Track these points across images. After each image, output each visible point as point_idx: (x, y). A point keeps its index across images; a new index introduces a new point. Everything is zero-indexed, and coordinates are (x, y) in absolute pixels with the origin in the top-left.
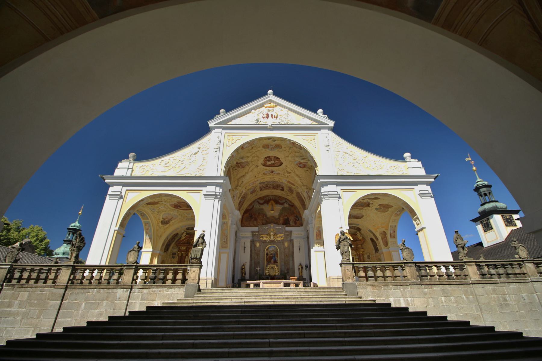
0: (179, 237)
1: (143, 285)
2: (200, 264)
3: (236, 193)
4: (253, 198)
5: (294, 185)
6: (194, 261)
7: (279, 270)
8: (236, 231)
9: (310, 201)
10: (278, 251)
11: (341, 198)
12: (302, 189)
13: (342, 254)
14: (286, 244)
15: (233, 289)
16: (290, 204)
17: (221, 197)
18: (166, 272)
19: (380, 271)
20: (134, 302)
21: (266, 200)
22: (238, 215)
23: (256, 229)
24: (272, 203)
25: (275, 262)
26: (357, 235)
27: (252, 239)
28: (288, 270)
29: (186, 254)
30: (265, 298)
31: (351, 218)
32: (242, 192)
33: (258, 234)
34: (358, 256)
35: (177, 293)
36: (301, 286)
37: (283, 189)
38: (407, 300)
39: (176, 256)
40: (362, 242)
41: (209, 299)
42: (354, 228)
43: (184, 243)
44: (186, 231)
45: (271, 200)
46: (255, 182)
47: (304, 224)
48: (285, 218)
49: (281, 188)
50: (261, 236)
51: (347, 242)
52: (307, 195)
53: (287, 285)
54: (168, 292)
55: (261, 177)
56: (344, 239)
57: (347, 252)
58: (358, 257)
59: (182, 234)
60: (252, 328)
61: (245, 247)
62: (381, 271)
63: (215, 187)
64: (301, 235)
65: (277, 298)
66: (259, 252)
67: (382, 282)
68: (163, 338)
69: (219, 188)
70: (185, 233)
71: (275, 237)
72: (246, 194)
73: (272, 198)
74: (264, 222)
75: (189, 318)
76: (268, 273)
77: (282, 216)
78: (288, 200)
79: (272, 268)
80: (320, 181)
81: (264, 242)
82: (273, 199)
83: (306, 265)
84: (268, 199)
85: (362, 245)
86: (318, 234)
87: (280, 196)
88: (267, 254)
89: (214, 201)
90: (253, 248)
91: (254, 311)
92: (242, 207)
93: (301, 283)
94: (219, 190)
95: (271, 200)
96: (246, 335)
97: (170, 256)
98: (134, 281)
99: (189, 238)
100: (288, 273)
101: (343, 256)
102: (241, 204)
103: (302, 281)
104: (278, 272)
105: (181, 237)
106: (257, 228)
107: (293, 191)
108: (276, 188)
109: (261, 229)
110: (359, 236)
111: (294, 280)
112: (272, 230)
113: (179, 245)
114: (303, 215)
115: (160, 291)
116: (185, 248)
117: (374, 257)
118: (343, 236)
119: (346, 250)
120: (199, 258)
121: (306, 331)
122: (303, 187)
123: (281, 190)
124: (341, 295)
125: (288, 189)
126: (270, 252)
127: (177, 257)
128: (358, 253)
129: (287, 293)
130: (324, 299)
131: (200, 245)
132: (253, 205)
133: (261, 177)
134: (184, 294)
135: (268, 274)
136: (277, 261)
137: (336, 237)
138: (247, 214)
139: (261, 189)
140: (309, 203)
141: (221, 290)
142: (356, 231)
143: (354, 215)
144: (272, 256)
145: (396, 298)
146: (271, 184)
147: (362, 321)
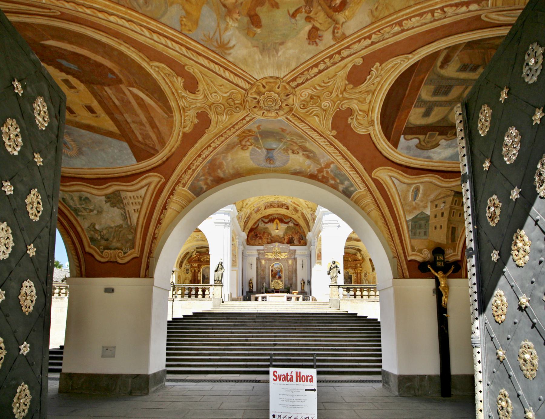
4: (259, 216)
10: (282, 268)
14: (290, 262)
21: (271, 219)
22: (244, 235)
23: (261, 247)
25: (280, 277)
28: (291, 284)
33: (263, 252)
43: (195, 261)
45: (275, 218)
47: (308, 244)
53: (289, 299)
59: (193, 252)
60: (264, 325)
70: (195, 251)
72: (251, 214)
73: (276, 217)
74: (269, 241)
75: (224, 319)
81: (269, 260)
85: (361, 264)
88: (272, 271)
92: (247, 226)
93: (301, 297)
95: (275, 218)
98: (174, 296)
100: (291, 287)
102: (246, 223)
106: (263, 247)
110: (359, 256)
112: (277, 249)
116: (197, 265)
123: (286, 209)
135: (273, 288)
138: (252, 233)
140: (313, 226)
142: (356, 251)
147: (333, 323)
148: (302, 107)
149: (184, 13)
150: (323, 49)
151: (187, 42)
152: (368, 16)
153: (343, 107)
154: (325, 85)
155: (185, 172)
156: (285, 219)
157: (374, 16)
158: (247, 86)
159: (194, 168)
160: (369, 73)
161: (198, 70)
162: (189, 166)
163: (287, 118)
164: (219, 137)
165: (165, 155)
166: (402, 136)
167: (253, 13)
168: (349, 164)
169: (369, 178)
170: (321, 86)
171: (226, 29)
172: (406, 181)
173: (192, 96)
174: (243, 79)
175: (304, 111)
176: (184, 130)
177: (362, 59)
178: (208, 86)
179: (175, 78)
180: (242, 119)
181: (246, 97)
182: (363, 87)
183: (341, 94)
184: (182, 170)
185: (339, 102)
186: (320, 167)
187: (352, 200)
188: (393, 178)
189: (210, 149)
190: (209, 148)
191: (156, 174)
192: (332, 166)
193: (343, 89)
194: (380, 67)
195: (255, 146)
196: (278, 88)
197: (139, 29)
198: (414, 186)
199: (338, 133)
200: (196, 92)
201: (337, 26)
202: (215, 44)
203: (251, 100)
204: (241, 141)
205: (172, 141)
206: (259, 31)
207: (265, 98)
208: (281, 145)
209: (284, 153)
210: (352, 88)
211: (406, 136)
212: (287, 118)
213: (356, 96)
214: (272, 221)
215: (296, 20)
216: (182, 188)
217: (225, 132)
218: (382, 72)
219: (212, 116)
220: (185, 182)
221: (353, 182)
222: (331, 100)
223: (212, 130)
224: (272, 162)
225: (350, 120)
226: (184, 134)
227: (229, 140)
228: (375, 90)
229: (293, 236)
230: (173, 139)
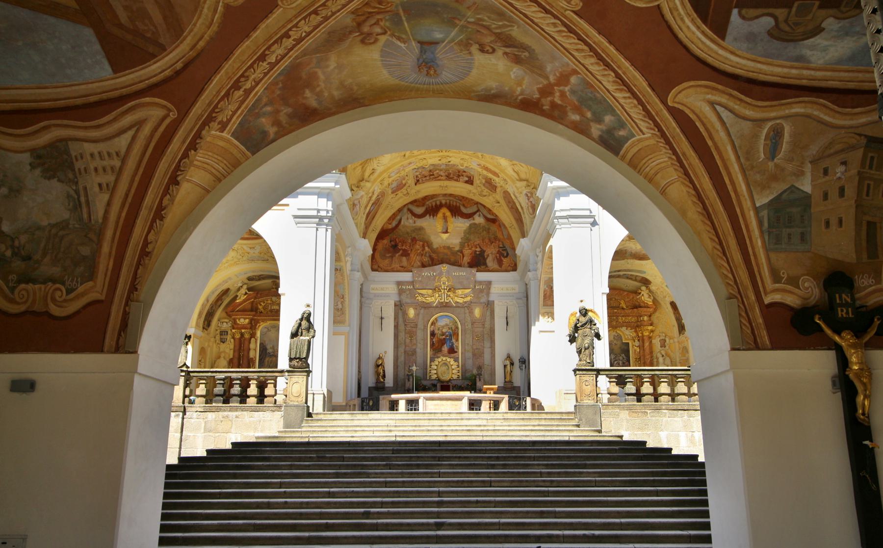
0: (232, 297)
1: (204, 405)
2: (308, 369)
3: (359, 196)
4: (401, 200)
5: (499, 177)
6: (296, 364)
7: (460, 369)
8: (362, 285)
9: (534, 217)
10: (457, 328)
11: (597, 224)
12: (516, 186)
13: (579, 352)
14: (477, 312)
15: (371, 413)
16: (489, 216)
17: (334, 221)
18: (245, 384)
19: (648, 383)
20: (192, 434)
22: (365, 247)
23: (406, 276)
24: (444, 214)
25: (452, 351)
26: (640, 293)
27: (397, 299)
28: (480, 368)
29: (251, 334)
30: (431, 430)
31: (628, 259)
32: (373, 193)
34: (639, 340)
35: (269, 419)
36: (504, 406)
37: (473, 181)
38: (692, 436)
39: (228, 339)
40: (651, 310)
41: (335, 431)
42: (634, 279)
43: (244, 311)
44: (246, 284)
46: (404, 167)
47: (520, 267)
48: (476, 251)
49: (467, 179)
50: (419, 294)
51: (591, 328)
53: (474, 405)
54: (252, 417)
55: (418, 155)
56: (585, 324)
57: (588, 348)
58: (638, 342)
59: (239, 290)
61: (382, 318)
62: (651, 385)
63: (316, 197)
64: (514, 291)
65: (452, 430)
66: (414, 329)
67: (650, 403)
68: (281, 485)
69: (326, 199)
70: (245, 287)
71: (451, 295)
72: (382, 194)
73: (443, 202)
74: (426, 259)
75: (311, 459)
76: (436, 376)
77: (468, 245)
78: (484, 206)
79: (445, 364)
80: (552, 185)
81: (427, 306)
82: (446, 203)
83: (521, 358)
84: (434, 204)
85: (650, 316)
86: (548, 293)
87: (463, 197)
88: (433, 334)
89: (317, 230)
90: (401, 320)
91: (413, 450)
94: (325, 205)
96: (404, 482)
97: (215, 338)
99: (255, 298)
100: (480, 375)
101: (581, 355)
102: (370, 217)
103: (507, 396)
104: (459, 374)
105: (237, 296)
107: (496, 187)
108: (455, 178)
109: (418, 277)
110: (646, 296)
111: (492, 392)
112: (444, 279)
113: (234, 313)
114: (518, 245)
115: (237, 417)
116: (247, 321)
117: (674, 342)
118: (583, 318)
119: (587, 345)
120: (304, 358)
121: (492, 479)
122: (519, 184)
123: (466, 182)
124: (569, 425)
125: (484, 181)
126: (439, 329)
127: (232, 340)
128: (640, 335)
129: (470, 421)
130: (533, 433)
131: (304, 333)
132: (398, 218)
133: (418, 155)
134: (282, 421)
136: (455, 350)
137: (571, 318)
139: (418, 181)
140: (532, 223)
141: (350, 416)
143: (633, 252)
144: (444, 337)
145: (672, 433)
146: (441, 170)
155: (227, 95)
159: (248, 85)
162: (238, 80)
164: (310, 14)
166: (735, 11)
168: (613, 74)
169: (661, 106)
172: (749, 113)
184: (219, 92)
186: (545, 82)
187: (623, 158)
188: (718, 107)
189: (287, 43)
190: (284, 40)
191: (157, 100)
192: (573, 80)
195: (393, 35)
198: (770, 124)
204: (359, 25)
208: (453, 34)
209: (461, 50)
211: (744, 11)
214: (433, 211)
216: (218, 133)
220: (225, 120)
221: (624, 117)
224: (432, 72)
227: (332, 22)
229: (484, 249)
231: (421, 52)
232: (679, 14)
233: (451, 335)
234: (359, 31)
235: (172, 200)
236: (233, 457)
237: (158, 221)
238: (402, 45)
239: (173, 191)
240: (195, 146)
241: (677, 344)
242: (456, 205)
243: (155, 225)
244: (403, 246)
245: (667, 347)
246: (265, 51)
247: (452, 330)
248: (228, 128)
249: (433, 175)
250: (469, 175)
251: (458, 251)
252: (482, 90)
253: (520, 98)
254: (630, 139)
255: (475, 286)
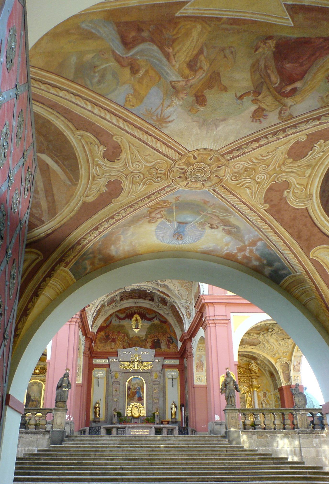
16: (163, 320)
24: (136, 318)
49: (150, 298)
52: (186, 311)
73: (136, 311)
77: (150, 336)
82: (137, 312)
84: (131, 312)
95: (135, 313)
108: (144, 297)
123: (150, 300)
125: (160, 300)
126: (132, 386)
144: (135, 390)
146: (136, 293)
148: (233, 179)
149: (132, 91)
150: (266, 126)
151: (127, 115)
152: (318, 101)
153: (280, 179)
154: (263, 158)
156: (149, 314)
157: (324, 102)
158: (175, 156)
160: (312, 148)
161: (126, 139)
163: (214, 190)
164: (127, 208)
165: (52, 226)
167: (199, 94)
168: (282, 241)
169: (307, 259)
170: (257, 159)
171: (169, 106)
173: (109, 164)
174: (175, 150)
175: (236, 182)
176: (85, 200)
177: (306, 136)
178: (132, 155)
179: (96, 146)
180: (161, 190)
181: (173, 167)
182: (303, 161)
183: (278, 167)
185: (276, 174)
186: (242, 244)
187: (281, 287)
189: (112, 221)
191: (33, 250)
192: (259, 244)
193: (281, 163)
194: (324, 144)
195: (166, 218)
196: (211, 159)
197: (83, 103)
199: (271, 206)
200: (116, 161)
201: (284, 108)
202: (154, 118)
203: (177, 170)
204: (150, 213)
205: (65, 211)
206: (202, 109)
207: (194, 169)
208: (197, 219)
210: (291, 162)
212: (214, 190)
213: (296, 169)
214: (130, 316)
215: (243, 102)
216: (63, 268)
217: (136, 203)
218: (325, 148)
219: (126, 185)
220: (69, 261)
222: (267, 173)
223: (123, 199)
225: (285, 193)
226: (84, 203)
227: (137, 211)
228: (316, 165)
229: (160, 338)
230: (68, 209)
231: (178, 227)
232: (317, 212)
233: (139, 389)
234: (149, 216)
235: (33, 305)
236: (27, 462)
237: (24, 317)
238: (169, 224)
239: (35, 300)
240: (50, 275)
241: (273, 395)
242: (143, 313)
243: (22, 319)
244: (112, 336)
245: (267, 397)
246: (98, 225)
247: (140, 386)
248: (69, 266)
249: (131, 296)
250: (151, 296)
251: (144, 339)
252: (204, 248)
253: (225, 252)
254: (288, 275)
255: (154, 360)
